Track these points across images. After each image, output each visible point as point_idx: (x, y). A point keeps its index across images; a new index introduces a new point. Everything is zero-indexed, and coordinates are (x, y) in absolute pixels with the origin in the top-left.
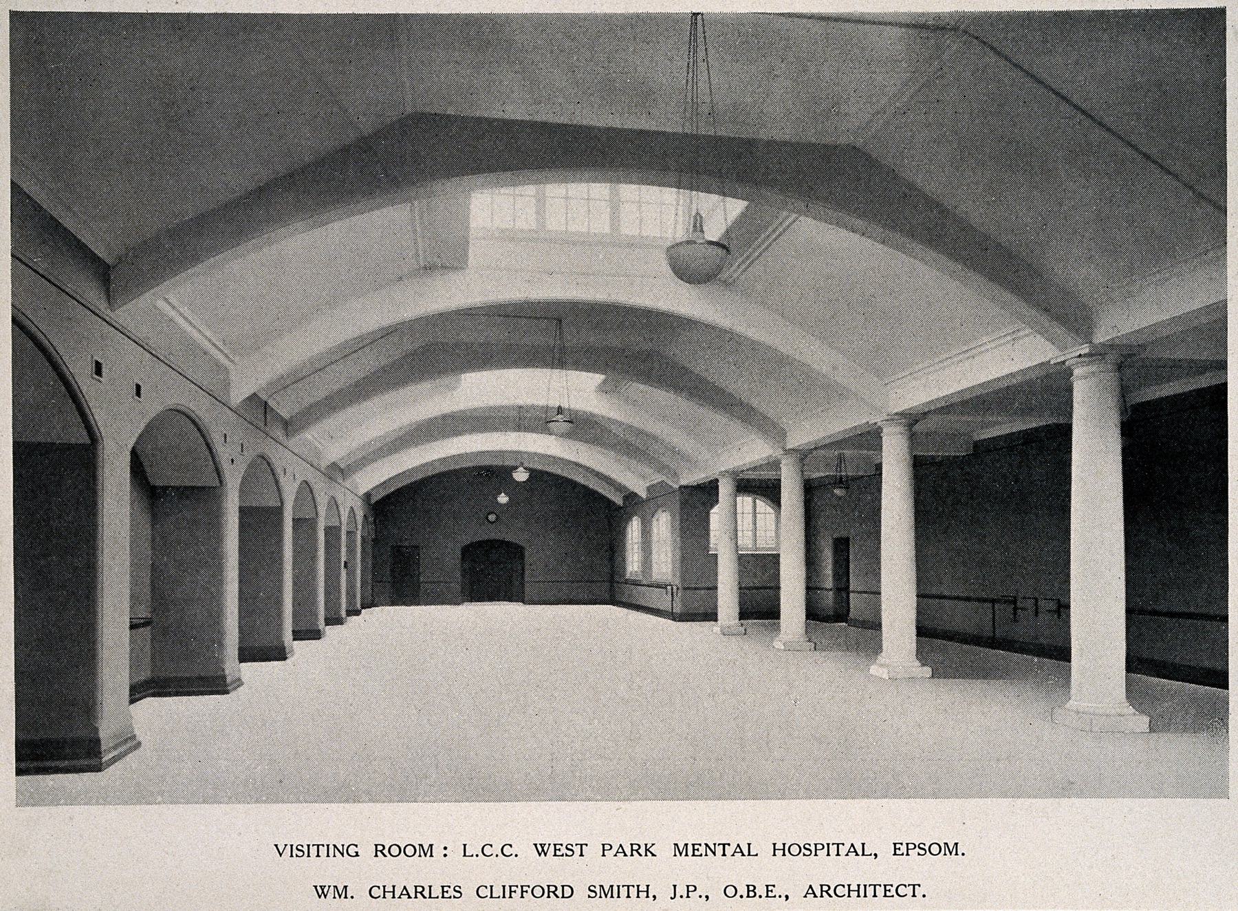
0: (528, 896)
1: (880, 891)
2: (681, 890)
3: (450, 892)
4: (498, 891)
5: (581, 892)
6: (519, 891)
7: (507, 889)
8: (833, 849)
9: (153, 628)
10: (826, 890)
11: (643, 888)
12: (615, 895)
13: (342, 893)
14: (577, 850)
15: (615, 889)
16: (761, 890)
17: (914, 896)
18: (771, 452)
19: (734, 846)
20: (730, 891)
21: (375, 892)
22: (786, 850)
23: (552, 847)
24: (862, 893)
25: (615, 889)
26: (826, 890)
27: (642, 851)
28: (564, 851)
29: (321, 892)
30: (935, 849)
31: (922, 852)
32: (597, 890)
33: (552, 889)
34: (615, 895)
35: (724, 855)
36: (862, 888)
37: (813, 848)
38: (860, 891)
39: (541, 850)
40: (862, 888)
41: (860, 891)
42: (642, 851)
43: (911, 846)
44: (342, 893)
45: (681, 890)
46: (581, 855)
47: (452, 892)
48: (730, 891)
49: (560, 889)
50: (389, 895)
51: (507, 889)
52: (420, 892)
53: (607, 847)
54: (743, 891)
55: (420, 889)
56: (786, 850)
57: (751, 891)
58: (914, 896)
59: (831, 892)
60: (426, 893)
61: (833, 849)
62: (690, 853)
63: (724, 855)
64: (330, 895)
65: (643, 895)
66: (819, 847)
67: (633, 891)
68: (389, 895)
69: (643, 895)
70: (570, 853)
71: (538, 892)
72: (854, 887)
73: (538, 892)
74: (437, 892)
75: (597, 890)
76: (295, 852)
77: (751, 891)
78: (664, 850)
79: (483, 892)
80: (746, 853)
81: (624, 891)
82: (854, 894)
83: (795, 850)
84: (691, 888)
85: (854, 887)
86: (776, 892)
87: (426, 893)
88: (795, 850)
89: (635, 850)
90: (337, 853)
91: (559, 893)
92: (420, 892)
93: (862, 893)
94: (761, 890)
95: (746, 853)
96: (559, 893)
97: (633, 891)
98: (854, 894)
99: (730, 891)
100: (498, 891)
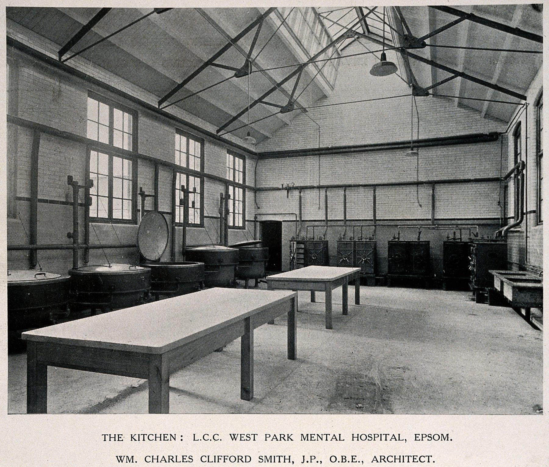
0: (227, 461)
1: (411, 459)
2: (307, 458)
3: (247, 459)
5: (255, 459)
6: (223, 458)
7: (217, 458)
8: (383, 437)
10: (383, 459)
11: (287, 457)
12: (273, 460)
13: (131, 459)
14: (252, 437)
16: (349, 459)
17: (429, 462)
20: (333, 459)
21: (148, 459)
22: (359, 437)
23: (239, 435)
24: (402, 460)
26: (383, 459)
27: (286, 438)
28: (245, 438)
29: (120, 459)
30: (436, 437)
31: (430, 439)
32: (264, 458)
33: (240, 458)
34: (273, 460)
36: (402, 458)
37: (373, 436)
38: (401, 459)
39: (233, 437)
40: (402, 458)
41: (401, 459)
42: (286, 438)
43: (424, 436)
44: (131, 459)
45: (307, 458)
46: (254, 440)
47: (187, 459)
48: (333, 459)
50: (155, 461)
51: (217, 458)
52: (171, 459)
53: (268, 436)
54: (339, 459)
55: (171, 458)
56: (359, 437)
58: (429, 462)
59: (386, 460)
60: (174, 460)
61: (383, 437)
62: (309, 438)
64: (125, 461)
65: (287, 461)
66: (376, 436)
67: (282, 459)
68: (155, 461)
69: (287, 461)
70: (248, 439)
71: (233, 459)
72: (397, 457)
73: (233, 459)
74: (180, 459)
75: (264, 458)
77: (344, 459)
78: (296, 437)
81: (406, 459)
83: (363, 437)
84: (313, 458)
86: (357, 459)
87: (174, 460)
88: (363, 437)
89: (282, 437)
91: (244, 460)
92: (171, 459)
93: (402, 460)
94: (349, 459)
96: (244, 460)
97: (282, 459)
99: (333, 459)
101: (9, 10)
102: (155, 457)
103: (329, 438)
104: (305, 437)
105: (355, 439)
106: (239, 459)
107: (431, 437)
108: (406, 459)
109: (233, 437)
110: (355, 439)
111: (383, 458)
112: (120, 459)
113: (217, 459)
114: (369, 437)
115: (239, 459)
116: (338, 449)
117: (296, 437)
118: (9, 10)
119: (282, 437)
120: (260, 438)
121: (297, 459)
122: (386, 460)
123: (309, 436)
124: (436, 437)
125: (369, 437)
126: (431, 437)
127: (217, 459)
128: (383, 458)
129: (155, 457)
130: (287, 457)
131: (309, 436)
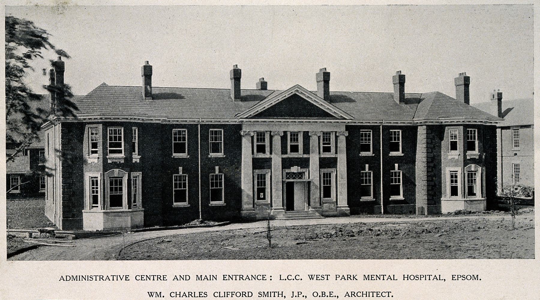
1: (375, 294)
3: (249, 294)
4: (222, 294)
5: (256, 295)
6: (231, 294)
8: (428, 277)
9: (457, 103)
10: (353, 294)
11: (280, 293)
13: (159, 295)
14: (326, 277)
15: (269, 293)
16: (327, 294)
18: (393, 92)
19: (387, 276)
20: (315, 294)
21: (173, 295)
22: (408, 277)
23: (315, 276)
24: (368, 295)
25: (269, 293)
26: (353, 294)
27: (352, 278)
28: (320, 278)
29: (151, 294)
30: (469, 277)
32: (262, 294)
33: (244, 293)
35: (384, 279)
36: (368, 293)
37: (419, 277)
38: (367, 294)
39: (311, 277)
40: (368, 293)
41: (367, 294)
42: (352, 278)
43: (459, 276)
44: (159, 295)
47: (203, 295)
48: (315, 294)
49: (247, 293)
50: (178, 296)
52: (190, 294)
53: (338, 276)
54: (320, 294)
56: (408, 277)
57: (323, 294)
59: (355, 295)
60: (193, 295)
61: (428, 277)
62: (370, 279)
63: (384, 279)
64: (154, 296)
65: (280, 296)
66: (422, 276)
67: (276, 294)
68: (178, 296)
69: (280, 296)
72: (365, 293)
73: (238, 294)
74: (197, 294)
75: (262, 294)
76: (89, 278)
77: (323, 294)
78: (360, 277)
79: (216, 295)
80: (392, 279)
81: (371, 294)
82: (364, 296)
83: (412, 278)
84: (300, 293)
85: (365, 293)
86: (334, 295)
87: (193, 295)
88: (412, 278)
89: (349, 277)
90: (253, 279)
91: (247, 295)
92: (190, 294)
93: (368, 295)
94: (327, 294)
95: (392, 279)
96: (247, 295)
97: (276, 294)
98: (364, 296)
99: (315, 294)
100: (222, 294)
101: (533, 257)
102: (178, 293)
103: (386, 278)
104: (366, 278)
105: (406, 279)
106: (243, 294)
107: (464, 278)
108: (371, 294)
109: (311, 277)
110: (406, 279)
111: (353, 293)
112: (151, 294)
113: (226, 294)
114: (416, 277)
115: (243, 294)
116: (265, 286)
117: (360, 277)
118: (533, 257)
119: (349, 277)
120: (332, 278)
121: (288, 294)
122: (355, 295)
123: (370, 277)
124: (469, 277)
125: (416, 277)
126: (464, 278)
127: (226, 294)
128: (353, 293)
129: (178, 293)
130: (280, 293)
131: (370, 277)
